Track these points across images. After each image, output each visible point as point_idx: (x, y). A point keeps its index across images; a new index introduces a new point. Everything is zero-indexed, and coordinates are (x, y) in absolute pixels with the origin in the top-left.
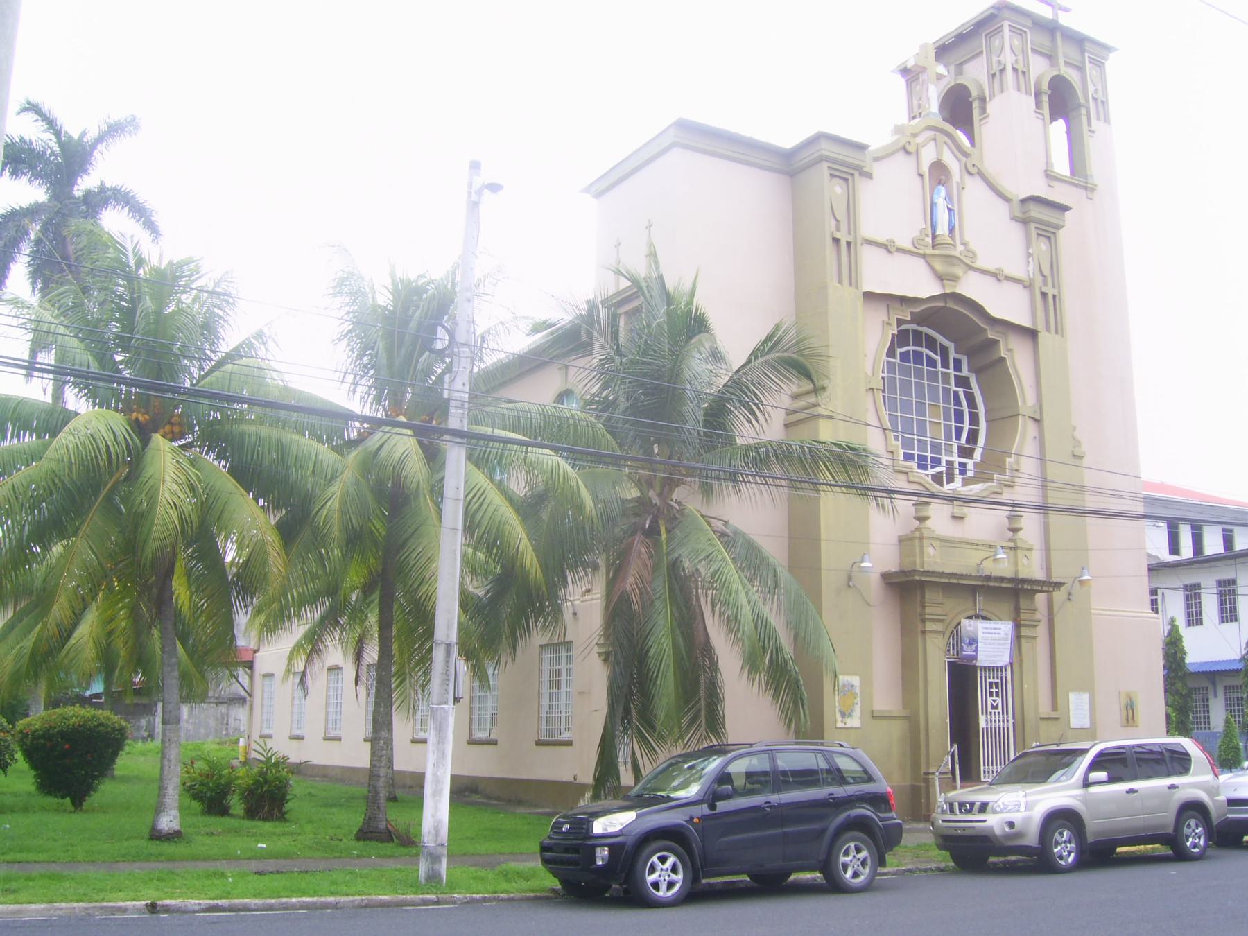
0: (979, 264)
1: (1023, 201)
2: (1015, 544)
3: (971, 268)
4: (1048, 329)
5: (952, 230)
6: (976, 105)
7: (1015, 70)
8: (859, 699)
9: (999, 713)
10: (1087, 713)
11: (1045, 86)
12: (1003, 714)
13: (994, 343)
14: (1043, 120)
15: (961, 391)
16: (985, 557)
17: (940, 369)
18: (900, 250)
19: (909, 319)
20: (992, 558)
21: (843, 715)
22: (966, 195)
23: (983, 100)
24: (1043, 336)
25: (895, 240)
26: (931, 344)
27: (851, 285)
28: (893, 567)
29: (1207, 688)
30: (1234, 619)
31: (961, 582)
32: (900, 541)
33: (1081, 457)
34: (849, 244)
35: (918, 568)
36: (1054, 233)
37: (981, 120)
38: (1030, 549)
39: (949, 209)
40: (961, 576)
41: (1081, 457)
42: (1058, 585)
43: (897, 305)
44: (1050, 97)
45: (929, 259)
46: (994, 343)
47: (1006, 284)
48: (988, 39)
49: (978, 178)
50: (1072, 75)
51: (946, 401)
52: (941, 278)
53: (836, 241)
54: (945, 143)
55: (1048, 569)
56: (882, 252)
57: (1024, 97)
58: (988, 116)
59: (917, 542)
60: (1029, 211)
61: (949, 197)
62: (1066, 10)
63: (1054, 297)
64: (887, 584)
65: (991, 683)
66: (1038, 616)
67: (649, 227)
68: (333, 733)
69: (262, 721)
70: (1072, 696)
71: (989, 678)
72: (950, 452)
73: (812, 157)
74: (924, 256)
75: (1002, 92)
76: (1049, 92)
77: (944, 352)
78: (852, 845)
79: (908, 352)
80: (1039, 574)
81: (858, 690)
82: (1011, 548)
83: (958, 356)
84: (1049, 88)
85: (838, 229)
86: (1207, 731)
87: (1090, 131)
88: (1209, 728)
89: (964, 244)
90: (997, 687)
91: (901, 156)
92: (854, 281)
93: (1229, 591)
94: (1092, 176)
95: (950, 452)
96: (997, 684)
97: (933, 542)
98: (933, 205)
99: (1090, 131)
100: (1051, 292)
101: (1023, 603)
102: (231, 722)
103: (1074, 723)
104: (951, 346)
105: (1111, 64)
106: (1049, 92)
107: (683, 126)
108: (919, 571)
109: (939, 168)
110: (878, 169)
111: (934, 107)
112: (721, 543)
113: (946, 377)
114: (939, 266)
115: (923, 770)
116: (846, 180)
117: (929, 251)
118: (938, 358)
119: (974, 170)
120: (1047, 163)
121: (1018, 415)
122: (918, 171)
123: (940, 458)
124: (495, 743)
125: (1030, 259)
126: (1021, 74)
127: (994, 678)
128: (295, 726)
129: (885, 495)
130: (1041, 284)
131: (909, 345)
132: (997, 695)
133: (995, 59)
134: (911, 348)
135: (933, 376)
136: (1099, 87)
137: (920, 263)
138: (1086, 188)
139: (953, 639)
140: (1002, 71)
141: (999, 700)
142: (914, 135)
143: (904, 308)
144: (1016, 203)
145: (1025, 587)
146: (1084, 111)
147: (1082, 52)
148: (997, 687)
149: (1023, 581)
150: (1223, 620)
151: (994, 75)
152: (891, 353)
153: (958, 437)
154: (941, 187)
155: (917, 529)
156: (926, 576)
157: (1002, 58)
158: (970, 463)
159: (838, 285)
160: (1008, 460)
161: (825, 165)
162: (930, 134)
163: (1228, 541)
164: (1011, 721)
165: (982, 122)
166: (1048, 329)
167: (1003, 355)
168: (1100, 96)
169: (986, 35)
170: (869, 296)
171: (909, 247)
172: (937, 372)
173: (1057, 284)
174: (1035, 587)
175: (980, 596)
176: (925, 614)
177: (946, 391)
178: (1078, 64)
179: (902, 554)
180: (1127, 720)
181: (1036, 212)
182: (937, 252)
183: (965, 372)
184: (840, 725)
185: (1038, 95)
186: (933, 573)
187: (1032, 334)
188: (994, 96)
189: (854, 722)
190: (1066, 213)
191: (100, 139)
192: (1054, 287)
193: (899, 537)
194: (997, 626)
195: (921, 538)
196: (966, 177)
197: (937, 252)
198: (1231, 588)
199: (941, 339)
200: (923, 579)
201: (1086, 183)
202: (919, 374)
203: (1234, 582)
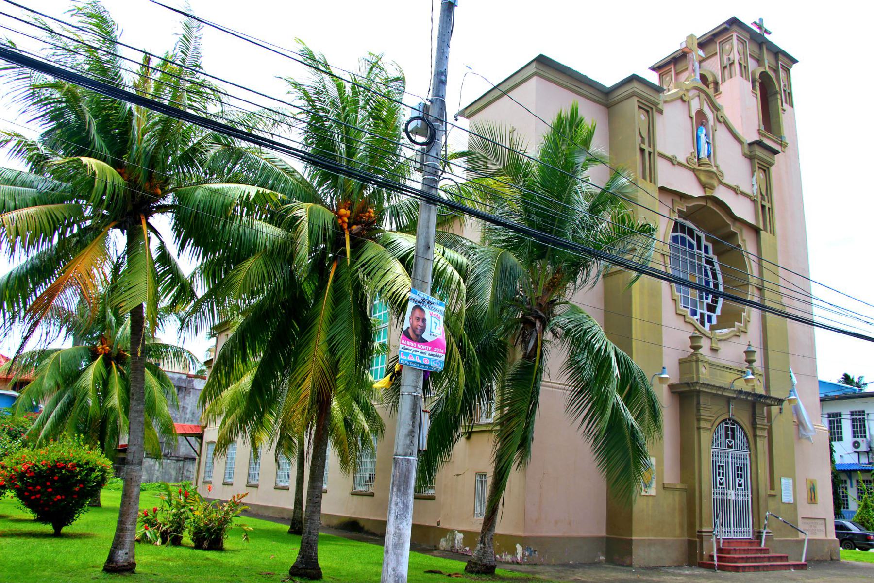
1: (750, 144)
5: (709, 156)
7: (740, 64)
10: (792, 492)
11: (757, 76)
13: (734, 234)
18: (680, 164)
19: (685, 210)
21: (646, 486)
22: (717, 133)
24: (762, 232)
26: (691, 232)
27: (651, 181)
28: (675, 380)
29: (846, 481)
36: (768, 168)
39: (708, 143)
43: (677, 199)
45: (697, 173)
46: (734, 234)
47: (740, 197)
50: (772, 74)
52: (704, 186)
53: (642, 150)
55: (767, 387)
56: (669, 164)
57: (745, 81)
59: (694, 363)
61: (707, 136)
62: (769, 33)
64: (672, 392)
65: (738, 468)
68: (252, 482)
69: (205, 472)
72: (702, 308)
73: (626, 93)
74: (694, 170)
76: (760, 81)
77: (699, 239)
79: (677, 236)
80: (763, 393)
88: (848, 508)
91: (679, 103)
92: (653, 180)
95: (702, 308)
98: (698, 138)
100: (767, 205)
102: (185, 472)
103: (785, 499)
104: (702, 235)
105: (794, 70)
106: (760, 81)
107: (542, 60)
109: (700, 114)
112: (535, 361)
115: (697, 529)
117: (696, 167)
118: (695, 243)
119: (721, 120)
124: (372, 495)
126: (743, 68)
128: (227, 476)
133: (725, 58)
134: (679, 234)
136: (786, 83)
140: (731, 64)
142: (687, 91)
144: (746, 146)
146: (779, 96)
147: (777, 60)
148: (723, 470)
151: (725, 67)
154: (702, 127)
155: (692, 355)
160: (743, 313)
161: (635, 99)
162: (696, 92)
164: (750, 496)
166: (765, 229)
170: (663, 190)
171: (684, 162)
173: (771, 201)
179: (682, 372)
181: (759, 152)
182: (702, 168)
183: (711, 254)
184: (644, 493)
185: (753, 82)
189: (652, 491)
193: (679, 359)
195: (697, 361)
196: (718, 125)
197: (702, 168)
198: (838, 419)
202: (684, 253)
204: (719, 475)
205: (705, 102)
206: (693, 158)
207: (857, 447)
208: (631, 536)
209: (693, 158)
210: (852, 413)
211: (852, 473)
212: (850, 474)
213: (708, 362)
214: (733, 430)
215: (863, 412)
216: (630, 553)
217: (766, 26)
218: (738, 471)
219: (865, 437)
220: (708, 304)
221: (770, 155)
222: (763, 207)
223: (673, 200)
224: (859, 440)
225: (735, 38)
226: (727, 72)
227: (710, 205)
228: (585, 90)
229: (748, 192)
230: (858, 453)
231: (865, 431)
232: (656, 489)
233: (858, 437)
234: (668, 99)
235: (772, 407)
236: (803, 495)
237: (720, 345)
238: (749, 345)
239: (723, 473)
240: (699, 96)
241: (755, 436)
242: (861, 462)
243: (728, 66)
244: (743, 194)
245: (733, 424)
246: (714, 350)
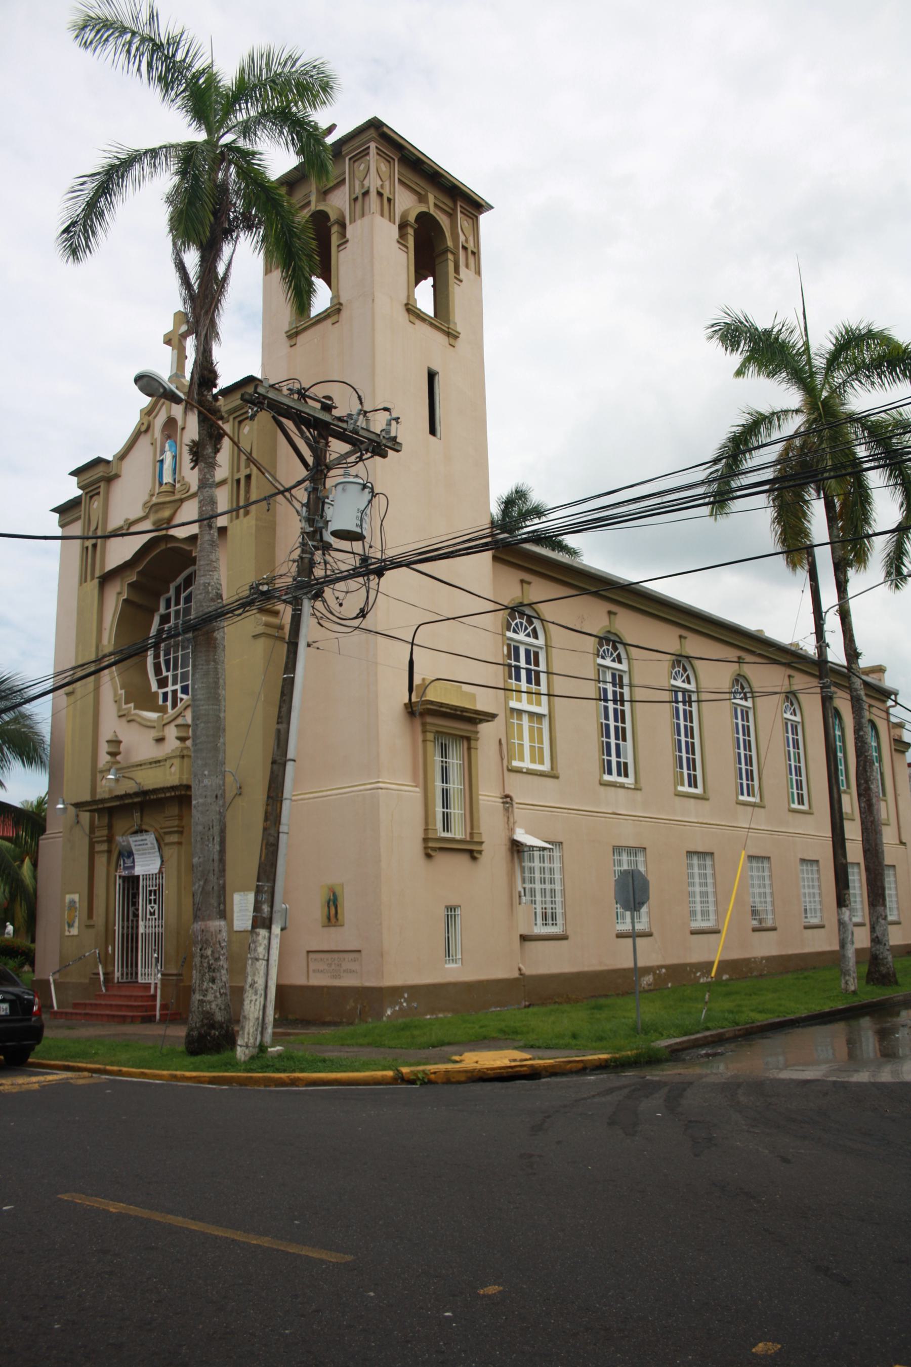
6: (335, 229)
7: (380, 194)
9: (155, 919)
11: (412, 219)
14: (407, 253)
23: (343, 226)
37: (339, 246)
44: (416, 231)
48: (352, 162)
50: (444, 220)
58: (347, 241)
65: (151, 891)
76: (416, 226)
87: (456, 278)
90: (150, 900)
96: (155, 891)
105: (484, 219)
120: (408, 297)
132: (155, 903)
133: (357, 183)
140: (366, 193)
141: (156, 907)
146: (450, 256)
148: (155, 895)
151: (356, 199)
168: (471, 246)
169: (350, 159)
180: (329, 918)
184: (67, 933)
185: (403, 227)
188: (378, 154)
191: (123, 456)
194: (143, 838)
204: (150, 903)
218: (150, 895)
226: (359, 204)
232: (79, 928)
239: (155, 900)
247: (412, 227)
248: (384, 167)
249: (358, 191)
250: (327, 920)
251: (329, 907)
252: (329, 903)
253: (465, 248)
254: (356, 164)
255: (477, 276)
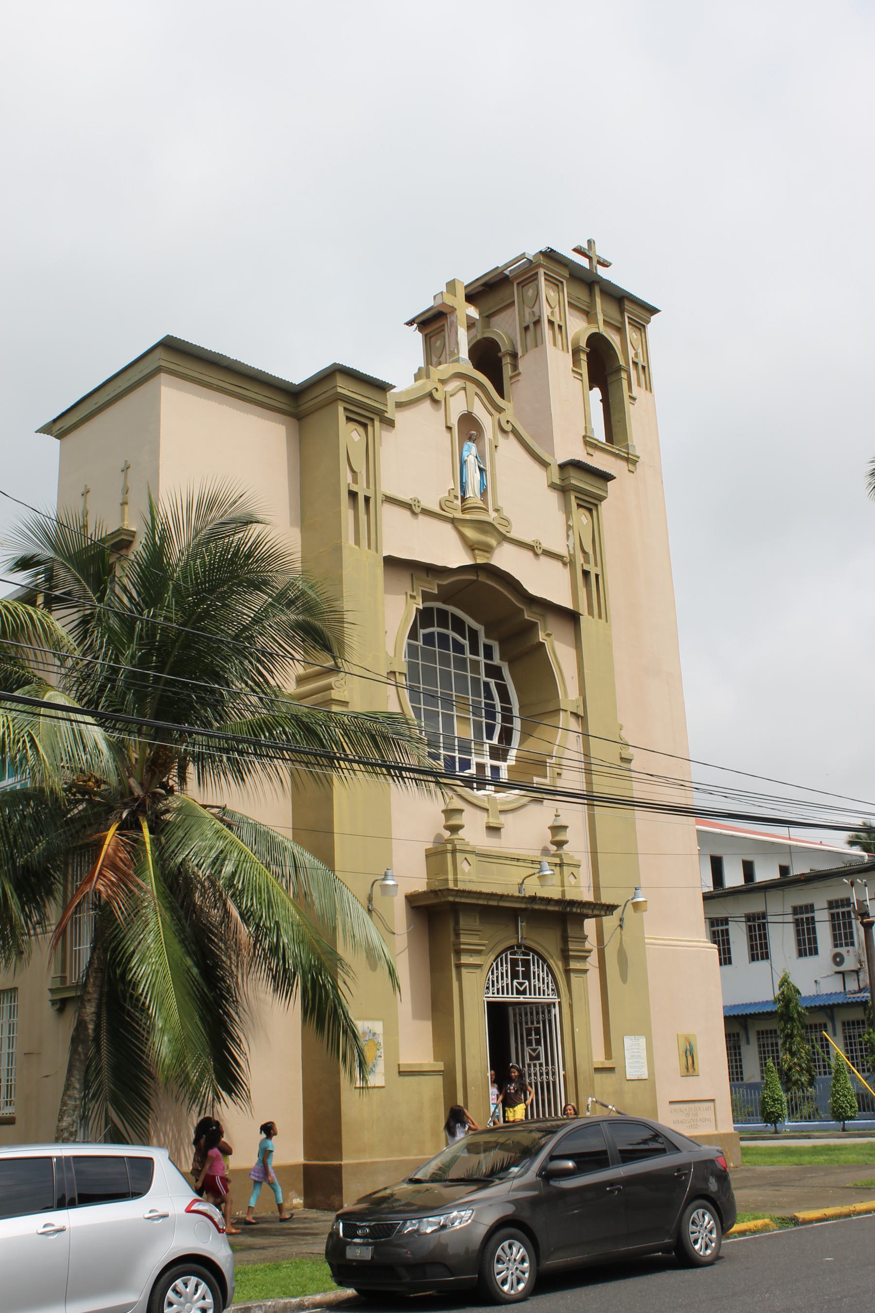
0: (514, 534)
1: (562, 467)
2: (561, 859)
3: (505, 538)
4: (591, 613)
5: (484, 493)
6: (507, 361)
7: (551, 323)
8: (382, 1050)
9: (541, 1065)
10: (645, 1061)
11: (583, 343)
12: (547, 1064)
13: (531, 627)
15: (492, 682)
16: (528, 874)
17: (468, 655)
18: (426, 512)
19: (436, 591)
20: (537, 875)
23: (514, 356)
24: (586, 621)
25: (541, 541)
26: (459, 626)
27: (369, 547)
28: (420, 885)
29: (738, 1034)
30: (766, 956)
31: (502, 904)
32: (427, 856)
33: (629, 761)
34: (367, 499)
35: (451, 885)
36: (596, 505)
37: (511, 378)
38: (578, 866)
39: (481, 470)
40: (502, 897)
41: (629, 761)
42: (610, 909)
44: (589, 355)
47: (543, 559)
48: (521, 288)
49: (511, 437)
50: (614, 339)
51: (476, 693)
52: (472, 547)
53: (353, 495)
54: (477, 394)
55: (597, 888)
57: (560, 353)
58: (520, 373)
59: (449, 856)
60: (569, 477)
61: (480, 457)
62: (605, 264)
63: (597, 576)
66: (587, 946)
67: (126, 469)
70: (628, 1041)
71: (527, 1023)
74: (453, 521)
75: (537, 346)
76: (588, 350)
77: (474, 636)
78: (506, 1288)
79: (432, 634)
80: (588, 896)
81: (381, 1039)
82: (556, 865)
83: (489, 642)
84: (587, 346)
85: (355, 481)
86: (740, 1082)
88: (742, 1079)
89: (497, 511)
91: (427, 404)
92: (374, 542)
93: (759, 925)
94: (634, 447)
97: (468, 856)
98: (463, 463)
99: (630, 397)
100: (593, 571)
101: (571, 931)
103: (631, 1074)
108: (452, 890)
110: (400, 417)
111: (464, 352)
113: (475, 665)
114: (470, 533)
116: (365, 426)
117: (459, 515)
118: (466, 643)
119: (508, 428)
121: (558, 710)
122: (446, 423)
123: (470, 760)
125: (570, 533)
127: (532, 1023)
129: (430, 779)
130: (582, 561)
131: (433, 626)
133: (527, 311)
134: (435, 629)
135: (461, 664)
136: (640, 351)
137: (448, 527)
138: (627, 460)
139: (493, 974)
141: (541, 1049)
143: (429, 579)
144: (555, 470)
145: (574, 910)
146: (624, 375)
147: (622, 311)
149: (572, 903)
150: (753, 958)
152: (413, 635)
153: (490, 737)
156: (461, 897)
157: (536, 309)
158: (503, 765)
159: (354, 546)
163: (749, 874)
165: (514, 380)
167: (541, 640)
168: (641, 362)
169: (518, 284)
170: (391, 562)
171: (437, 509)
172: (466, 659)
173: (599, 560)
174: (585, 911)
175: (522, 922)
176: (460, 944)
177: (476, 681)
178: (619, 325)
180: (687, 1069)
181: (577, 480)
182: (467, 517)
185: (576, 352)
186: (469, 894)
187: (571, 617)
190: (608, 483)
192: (596, 565)
193: (426, 850)
195: (454, 851)
199: (470, 621)
200: (458, 900)
201: (628, 454)
202: (445, 660)
203: (764, 916)
205: (476, 399)
206: (452, 498)
207: (838, 964)
208: (341, 1160)
209: (452, 498)
210: (832, 905)
211: (749, 1021)
212: (832, 1012)
213: (473, 852)
214: (526, 963)
215: (812, 906)
216: (338, 1189)
217: (600, 251)
219: (852, 944)
220: (492, 748)
221: (598, 483)
222: (586, 574)
223: (412, 575)
224: (843, 950)
225: (542, 278)
227: (483, 579)
228: (254, 392)
229: (562, 551)
230: (842, 973)
231: (851, 934)
233: (841, 945)
234: (403, 399)
235: (604, 918)
236: (674, 1062)
237: (503, 819)
238: (557, 816)
240: (464, 389)
241: (567, 972)
242: (847, 990)
243: (532, 326)
244: (548, 554)
245: (525, 954)
246: (494, 830)
247: (584, 351)
248: (552, 294)
249: (529, 320)
250: (686, 1070)
251: (687, 1057)
252: (686, 1053)
253: (635, 364)
254: (525, 288)
255: (648, 393)
